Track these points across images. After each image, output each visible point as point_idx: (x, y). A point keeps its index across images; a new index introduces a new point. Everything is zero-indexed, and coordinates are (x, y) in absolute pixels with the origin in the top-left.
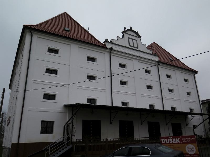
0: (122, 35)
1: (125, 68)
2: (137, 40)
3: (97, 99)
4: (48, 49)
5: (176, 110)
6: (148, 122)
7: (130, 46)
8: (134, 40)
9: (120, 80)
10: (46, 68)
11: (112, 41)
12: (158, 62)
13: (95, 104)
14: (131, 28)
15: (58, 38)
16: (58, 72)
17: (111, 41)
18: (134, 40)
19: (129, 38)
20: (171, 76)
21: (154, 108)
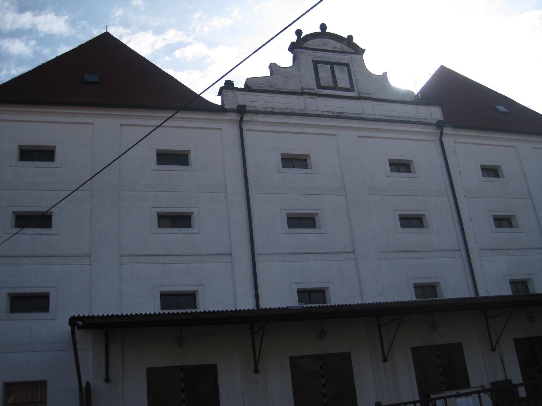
0: (290, 55)
1: (306, 167)
2: (347, 65)
3: (328, 288)
4: (283, 159)
5: (531, 292)
6: (149, 370)
7: (319, 87)
8: (335, 67)
9: (159, 210)
10: (158, 213)
11: (250, 85)
12: (440, 125)
13: (325, 305)
14: (323, 27)
15: (44, 110)
16: (195, 221)
17: (246, 85)
18: (335, 67)
19: (316, 63)
20: (499, 167)
21: (439, 294)
